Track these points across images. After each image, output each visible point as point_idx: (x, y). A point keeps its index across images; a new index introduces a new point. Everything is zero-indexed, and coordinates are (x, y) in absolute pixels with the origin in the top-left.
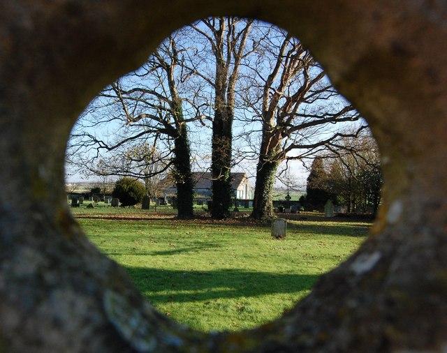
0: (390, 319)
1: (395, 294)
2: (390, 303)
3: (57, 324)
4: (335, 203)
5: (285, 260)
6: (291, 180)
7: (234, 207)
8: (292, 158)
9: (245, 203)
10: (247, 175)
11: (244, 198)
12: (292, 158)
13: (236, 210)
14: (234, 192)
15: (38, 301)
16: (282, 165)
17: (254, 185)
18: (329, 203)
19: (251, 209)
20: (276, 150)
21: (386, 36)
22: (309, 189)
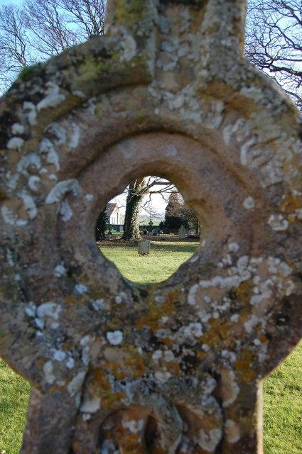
0: (200, 273)
1: (201, 267)
2: (200, 269)
3: (111, 277)
4: (187, 227)
5: (149, 272)
6: (153, 210)
7: (108, 231)
8: (154, 192)
9: (117, 227)
10: (119, 205)
11: (116, 224)
12: (154, 192)
13: (110, 233)
14: (108, 219)
15: (106, 271)
16: (145, 198)
17: (124, 214)
18: (182, 227)
19: (122, 232)
20: (142, 186)
21: (199, 197)
22: (167, 217)
